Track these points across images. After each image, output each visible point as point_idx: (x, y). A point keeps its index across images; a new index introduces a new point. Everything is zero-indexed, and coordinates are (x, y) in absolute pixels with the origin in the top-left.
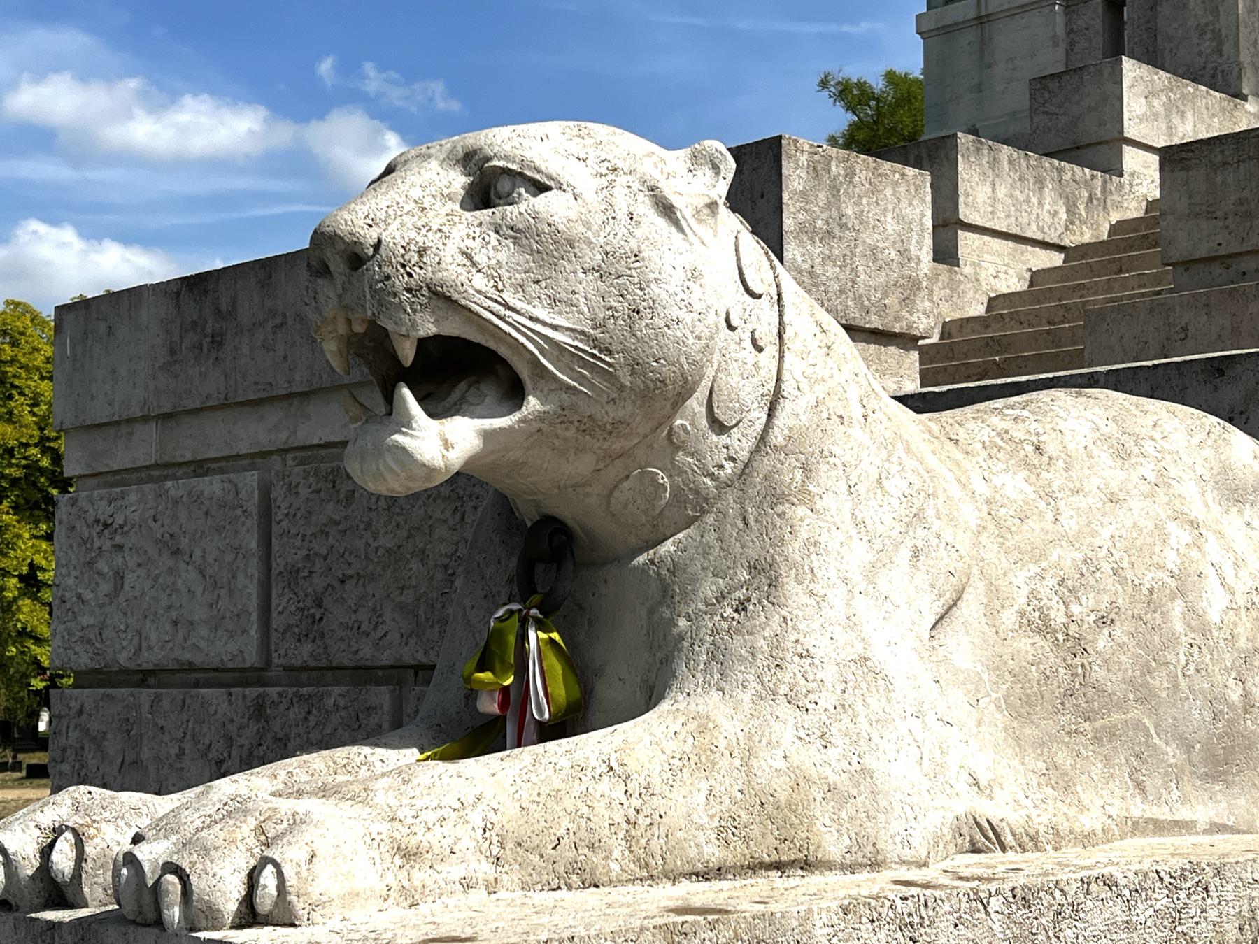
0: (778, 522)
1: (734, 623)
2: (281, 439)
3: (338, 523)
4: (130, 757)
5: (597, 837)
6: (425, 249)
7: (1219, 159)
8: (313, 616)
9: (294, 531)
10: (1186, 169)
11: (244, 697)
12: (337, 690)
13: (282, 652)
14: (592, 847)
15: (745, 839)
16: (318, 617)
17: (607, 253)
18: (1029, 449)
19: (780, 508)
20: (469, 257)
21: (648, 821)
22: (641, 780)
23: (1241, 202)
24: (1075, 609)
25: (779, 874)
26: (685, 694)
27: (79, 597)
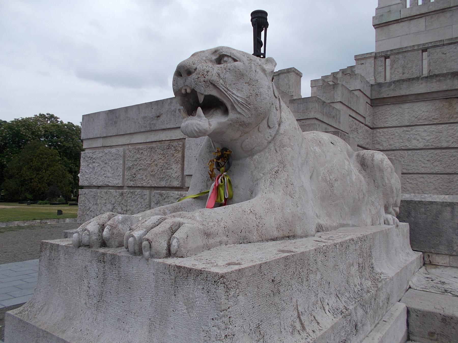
0: (285, 151)
1: (276, 176)
2: (128, 142)
3: (139, 158)
4: (95, 203)
5: (250, 230)
6: (209, 71)
7: (299, 103)
8: (133, 176)
9: (130, 160)
10: (294, 104)
11: (119, 192)
12: (138, 191)
13: (127, 183)
14: (249, 232)
15: (283, 230)
16: (134, 177)
17: (250, 79)
18: (319, 142)
19: (285, 148)
20: (219, 75)
21: (262, 225)
22: (259, 215)
23: (303, 110)
24: (331, 177)
25: (288, 239)
26: (264, 193)
27: (86, 171)
